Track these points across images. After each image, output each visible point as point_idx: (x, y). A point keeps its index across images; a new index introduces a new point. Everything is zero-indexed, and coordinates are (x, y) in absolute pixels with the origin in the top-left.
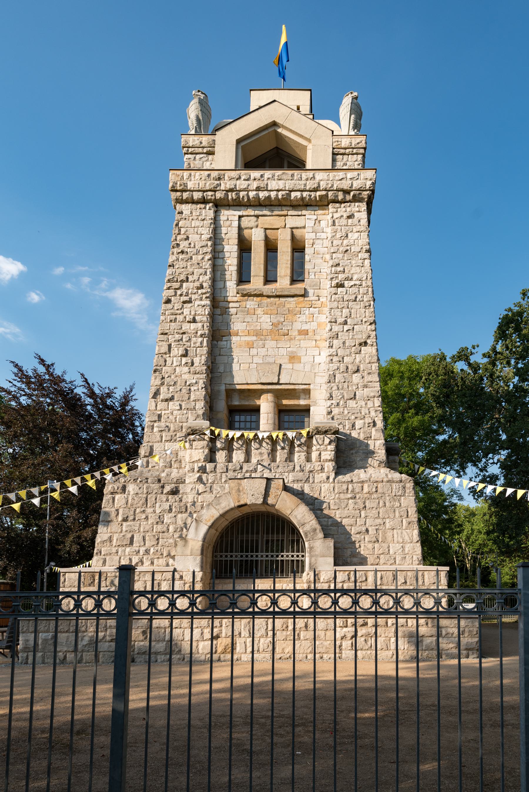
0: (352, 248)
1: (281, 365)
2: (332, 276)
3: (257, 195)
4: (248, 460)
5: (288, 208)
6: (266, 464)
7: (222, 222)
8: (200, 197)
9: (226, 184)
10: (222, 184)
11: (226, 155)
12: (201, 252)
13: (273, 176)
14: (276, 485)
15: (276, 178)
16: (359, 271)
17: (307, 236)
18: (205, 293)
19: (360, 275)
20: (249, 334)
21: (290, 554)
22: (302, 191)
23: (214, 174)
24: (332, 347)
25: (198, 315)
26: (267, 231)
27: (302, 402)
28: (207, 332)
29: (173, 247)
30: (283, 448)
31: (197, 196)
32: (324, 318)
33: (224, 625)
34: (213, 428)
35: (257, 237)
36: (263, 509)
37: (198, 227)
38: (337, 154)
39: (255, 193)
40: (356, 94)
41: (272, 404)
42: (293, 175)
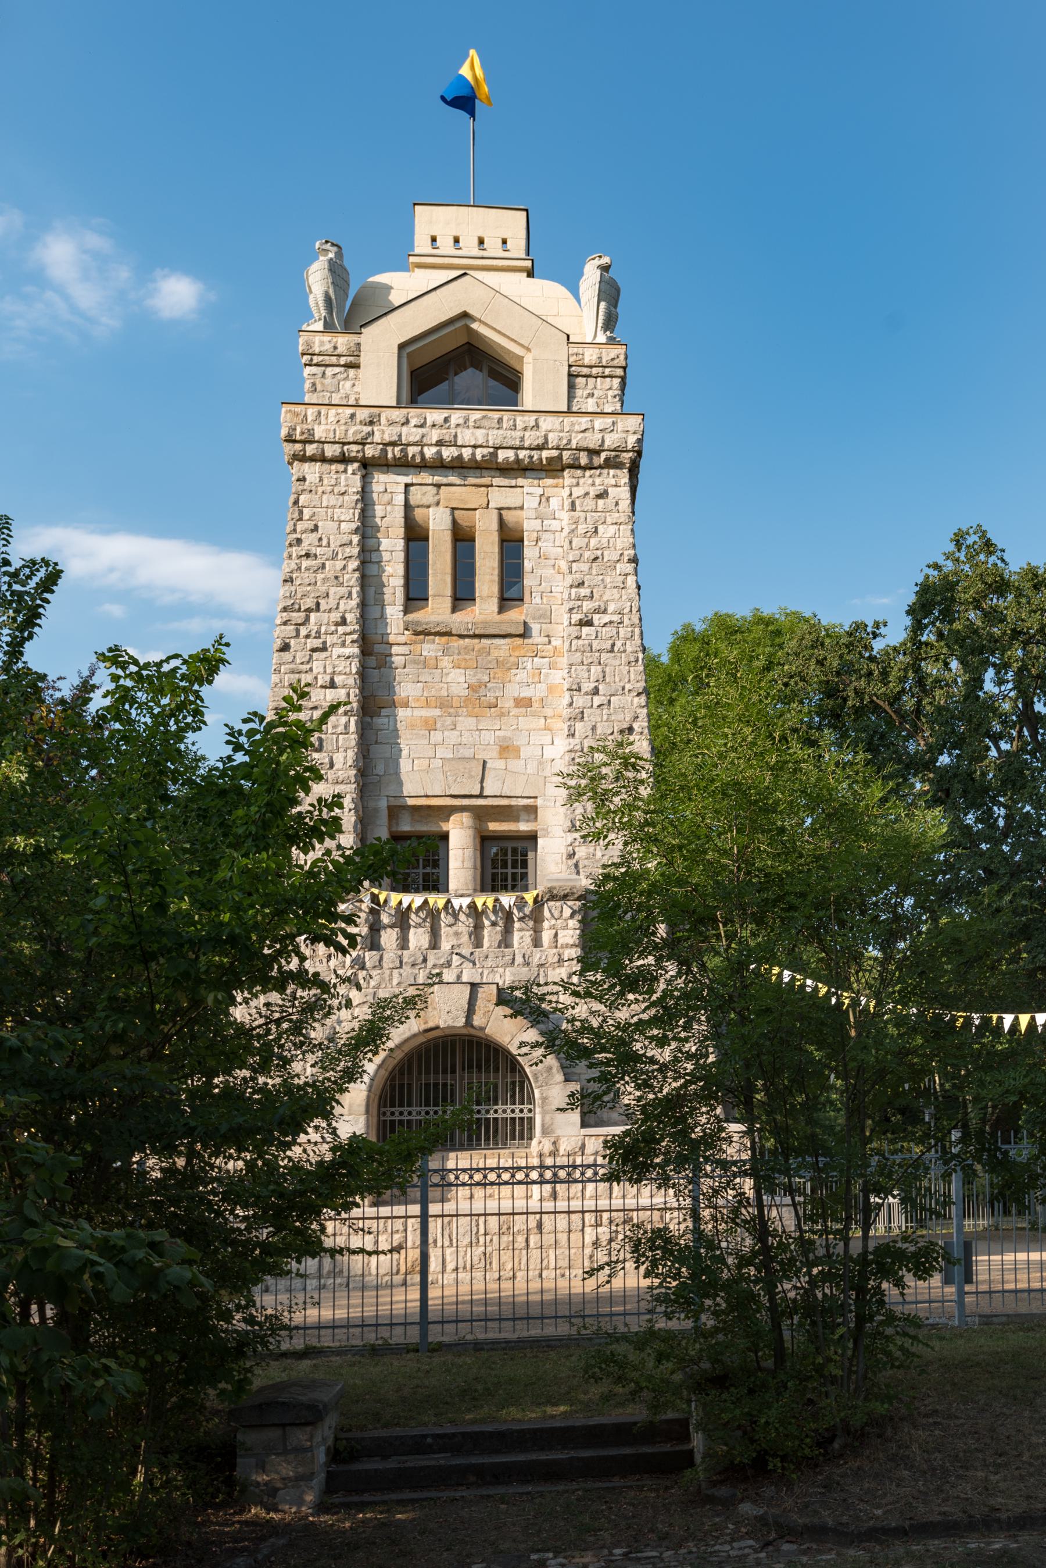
0: (606, 553)
1: (485, 762)
2: (571, 604)
3: (439, 453)
4: (434, 945)
5: (493, 473)
6: (466, 952)
7: (375, 496)
8: (337, 454)
9: (383, 432)
10: (376, 433)
11: (379, 378)
12: (340, 556)
13: (466, 420)
14: (487, 995)
15: (471, 424)
16: (617, 596)
17: (527, 525)
18: (350, 634)
19: (619, 604)
20: (428, 705)
21: (510, 1107)
22: (517, 449)
23: (362, 414)
24: (573, 735)
25: (340, 674)
26: (456, 512)
27: (523, 827)
28: (355, 705)
29: (291, 545)
30: (494, 924)
31: (330, 451)
32: (559, 677)
33: (410, 1229)
34: (376, 891)
35: (438, 523)
36: (464, 1031)
37: (333, 507)
38: (577, 376)
39: (434, 450)
40: (606, 260)
41: (470, 832)
42: (500, 421)
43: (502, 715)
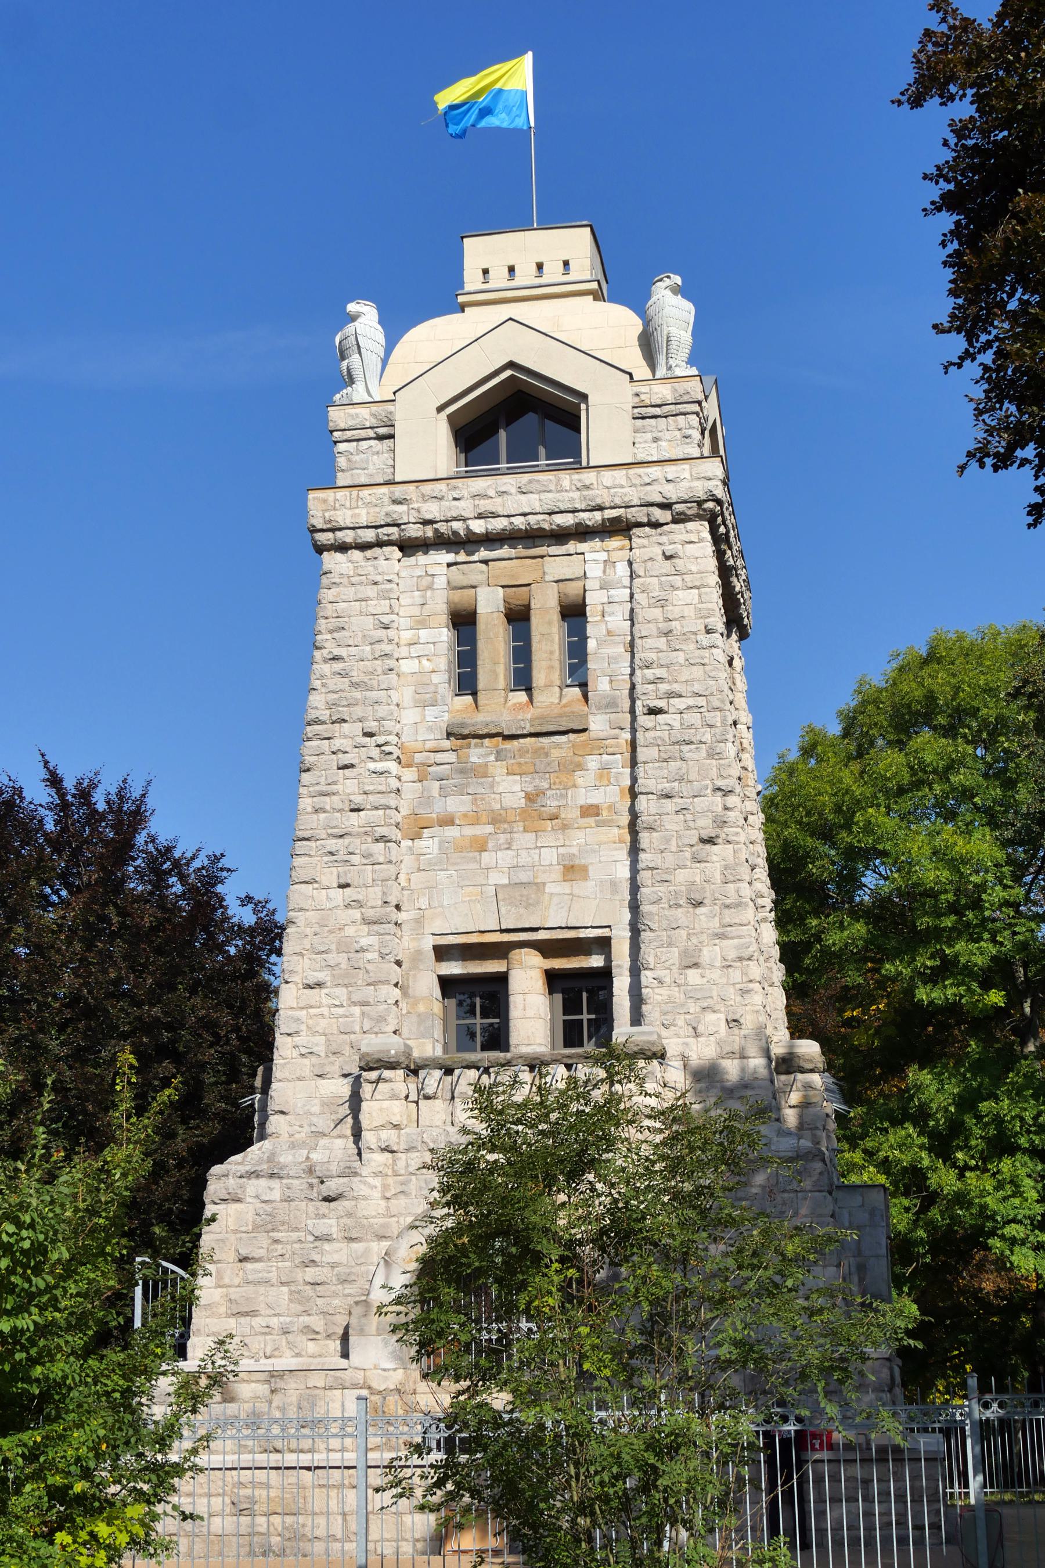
27: (596, 961)
35: (490, 605)
43: (565, 827)
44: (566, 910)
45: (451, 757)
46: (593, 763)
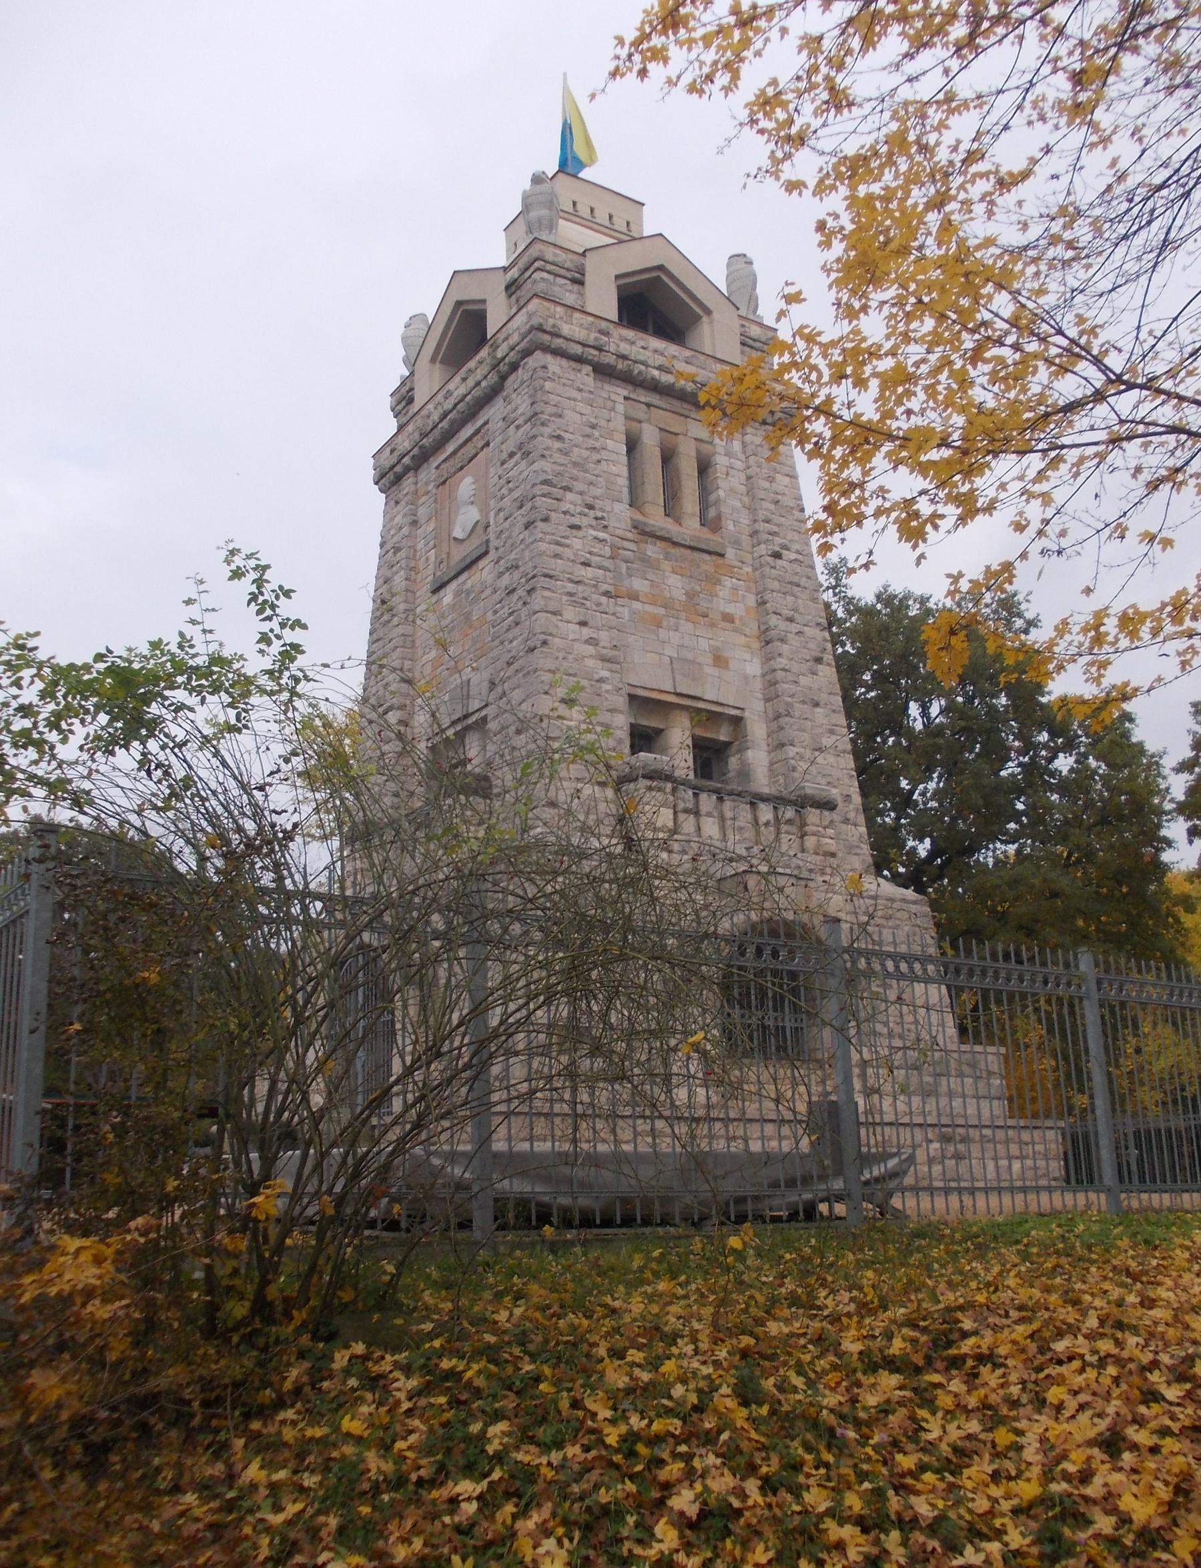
35: (650, 439)
44: (716, 689)
45: (632, 546)
46: (728, 582)
